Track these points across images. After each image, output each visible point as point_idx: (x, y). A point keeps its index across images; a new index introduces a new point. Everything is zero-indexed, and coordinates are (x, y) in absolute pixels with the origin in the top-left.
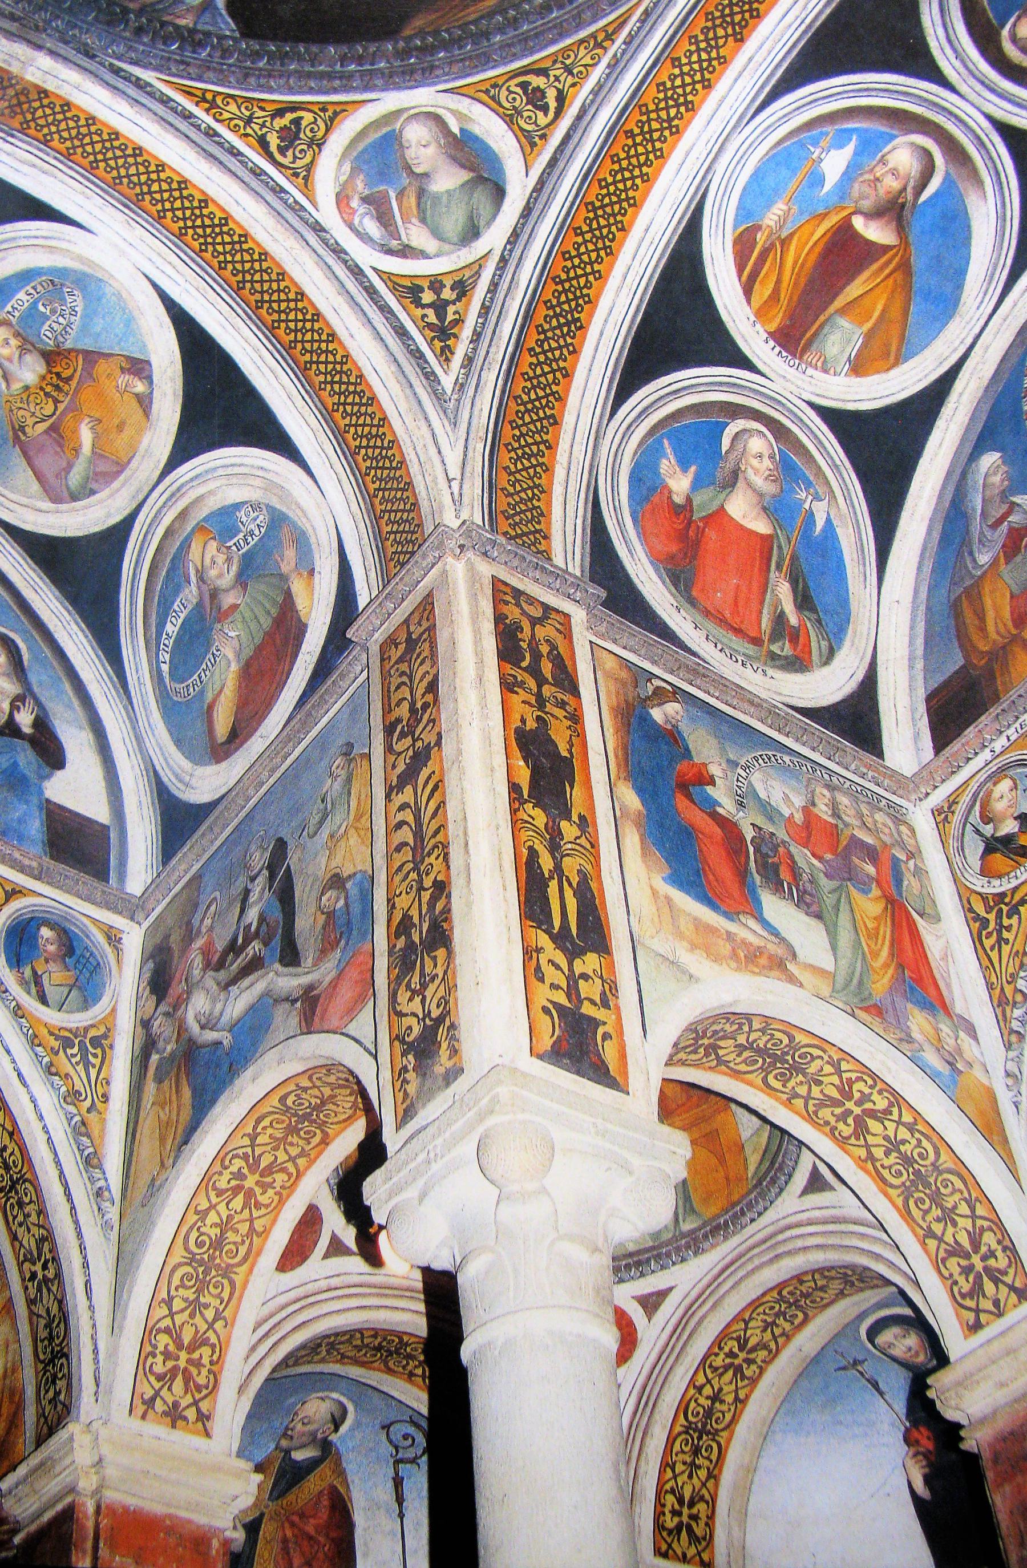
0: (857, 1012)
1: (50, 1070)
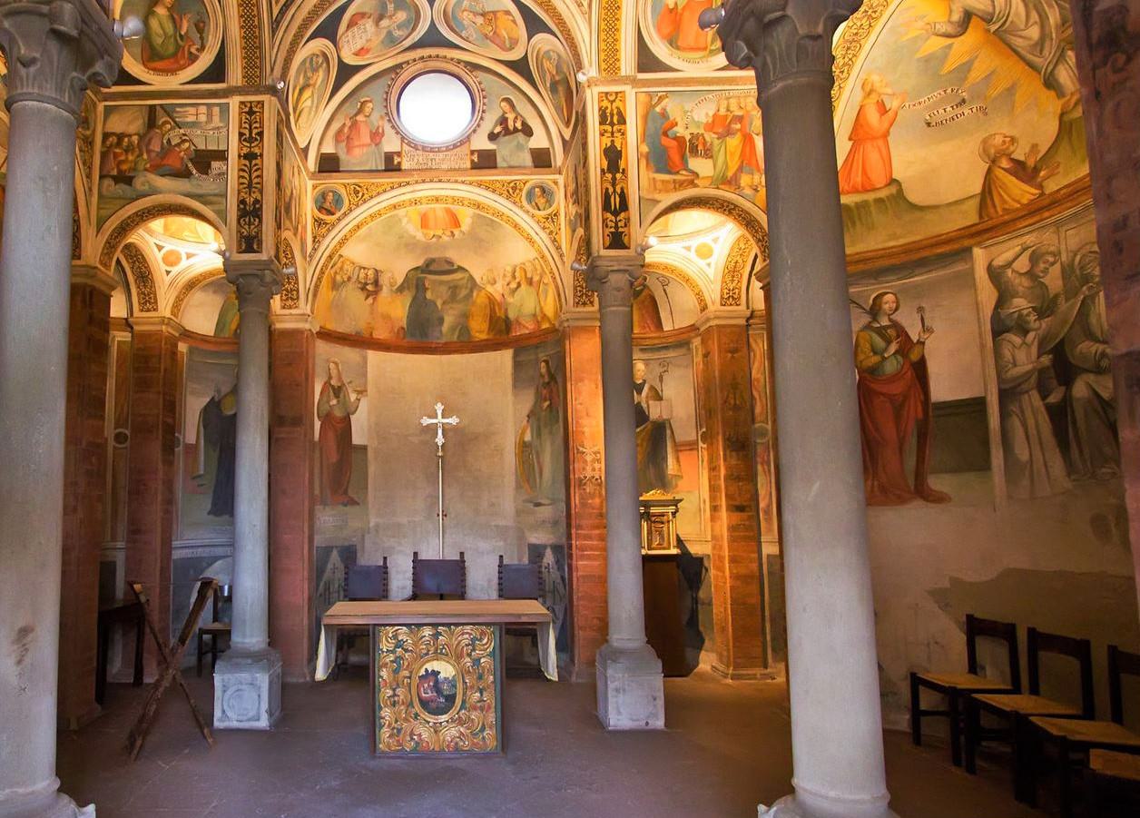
0: (720, 186)
1: (544, 228)
